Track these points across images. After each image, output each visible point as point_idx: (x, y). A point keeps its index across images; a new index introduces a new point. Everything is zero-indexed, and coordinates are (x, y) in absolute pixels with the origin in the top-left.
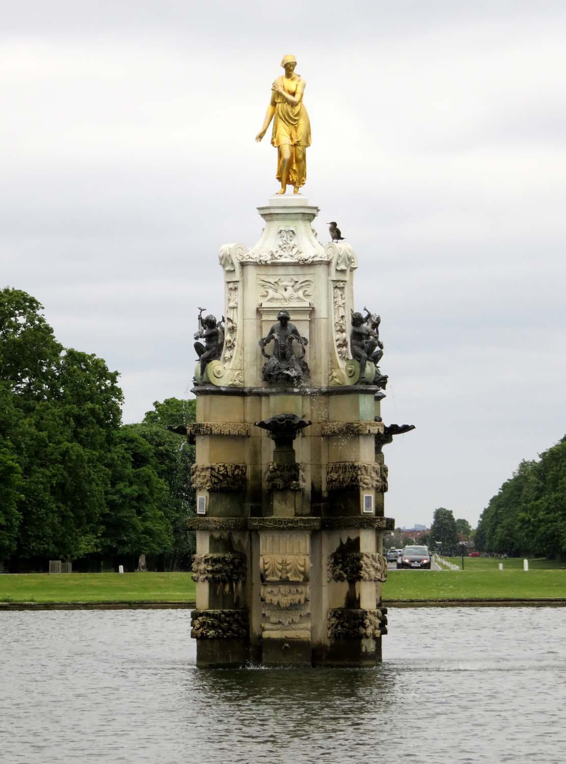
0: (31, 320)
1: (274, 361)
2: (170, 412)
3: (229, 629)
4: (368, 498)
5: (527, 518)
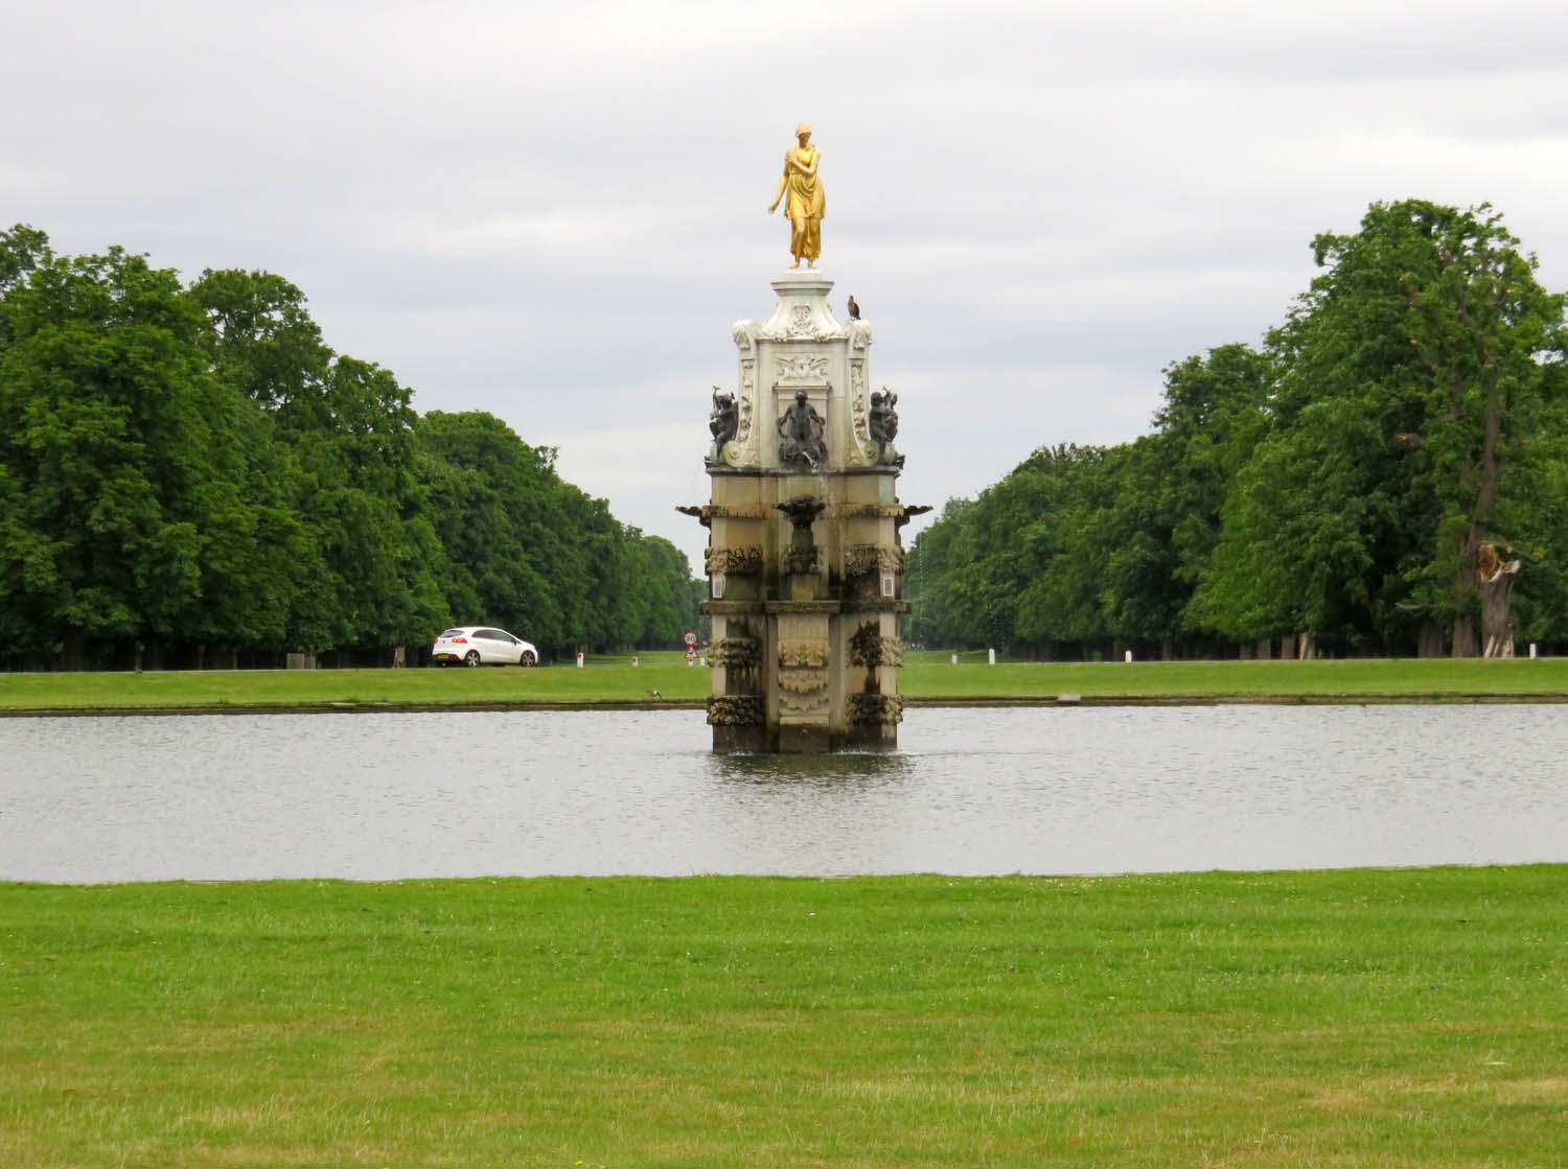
0: (290, 317)
1: (792, 442)
2: (432, 432)
3: (746, 715)
4: (888, 582)
5: (962, 590)
